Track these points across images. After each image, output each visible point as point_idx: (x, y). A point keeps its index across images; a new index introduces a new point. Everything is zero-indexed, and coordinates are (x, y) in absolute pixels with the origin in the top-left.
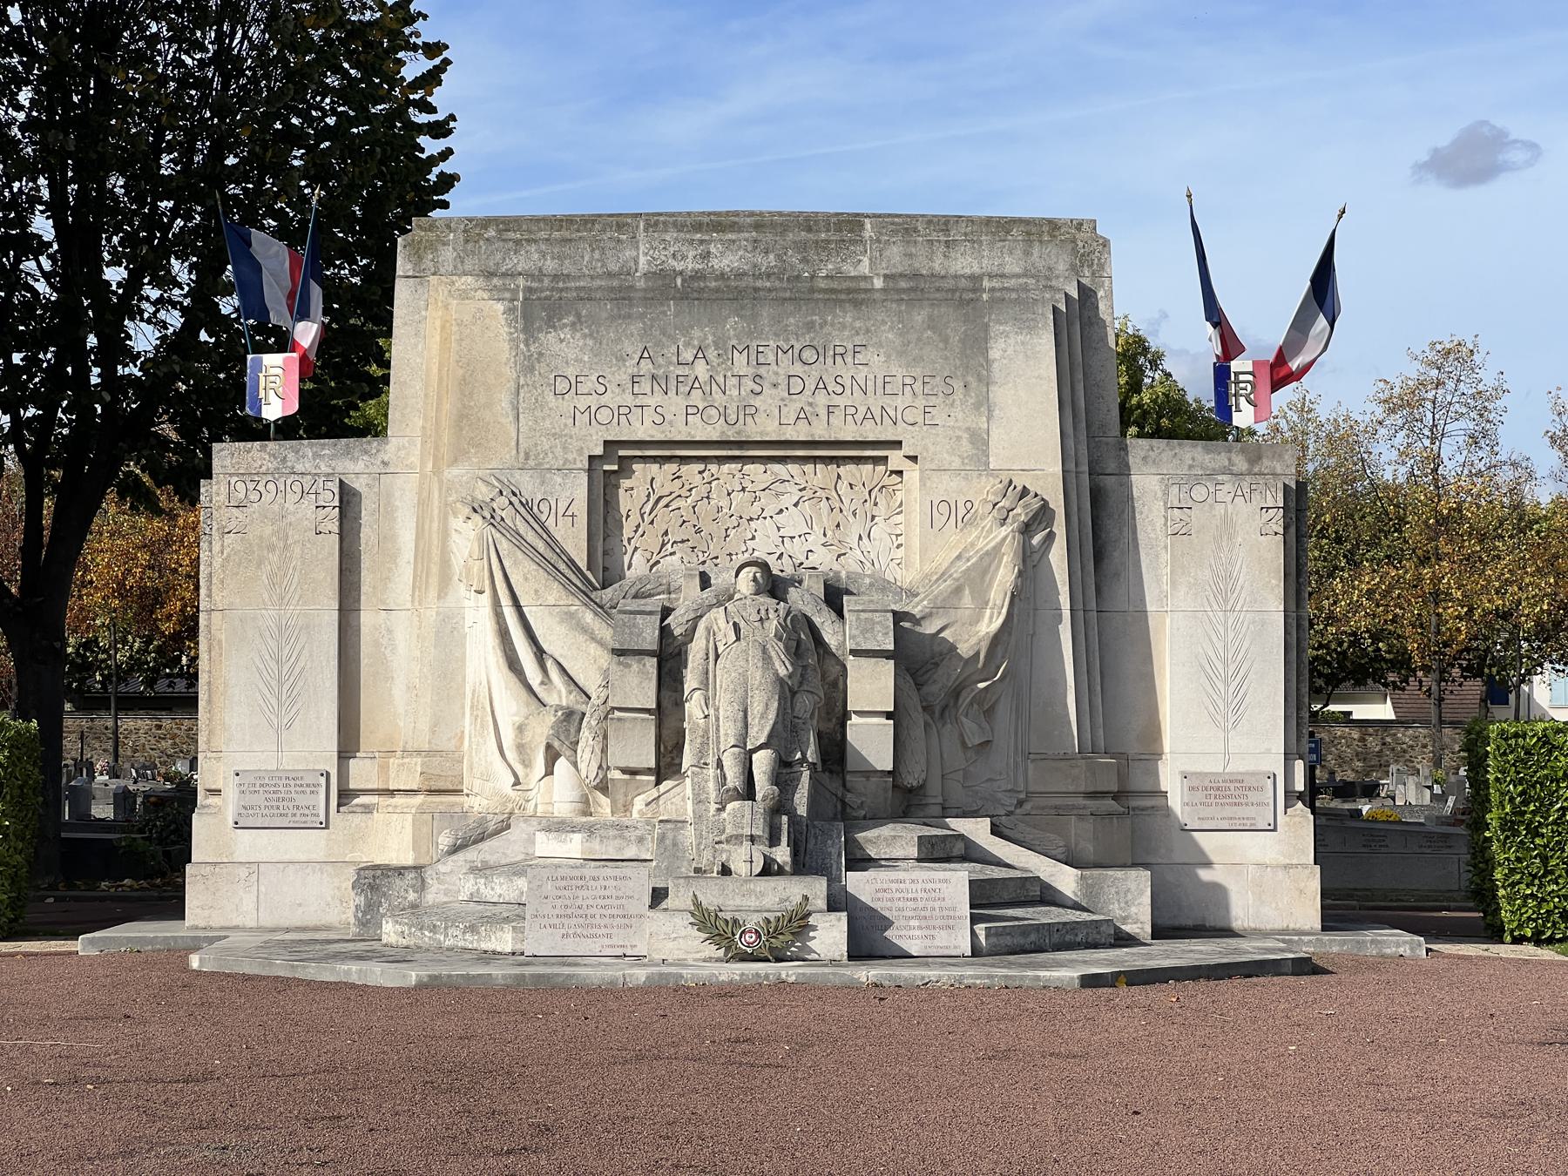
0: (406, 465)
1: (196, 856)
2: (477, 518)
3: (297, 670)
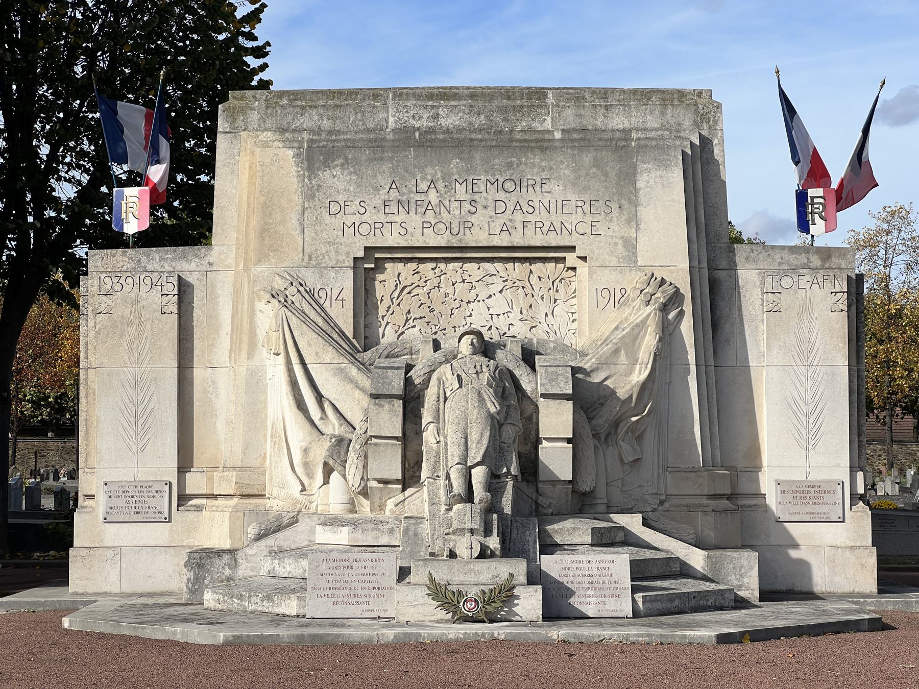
0: (224, 266)
2: (275, 302)
3: (148, 410)
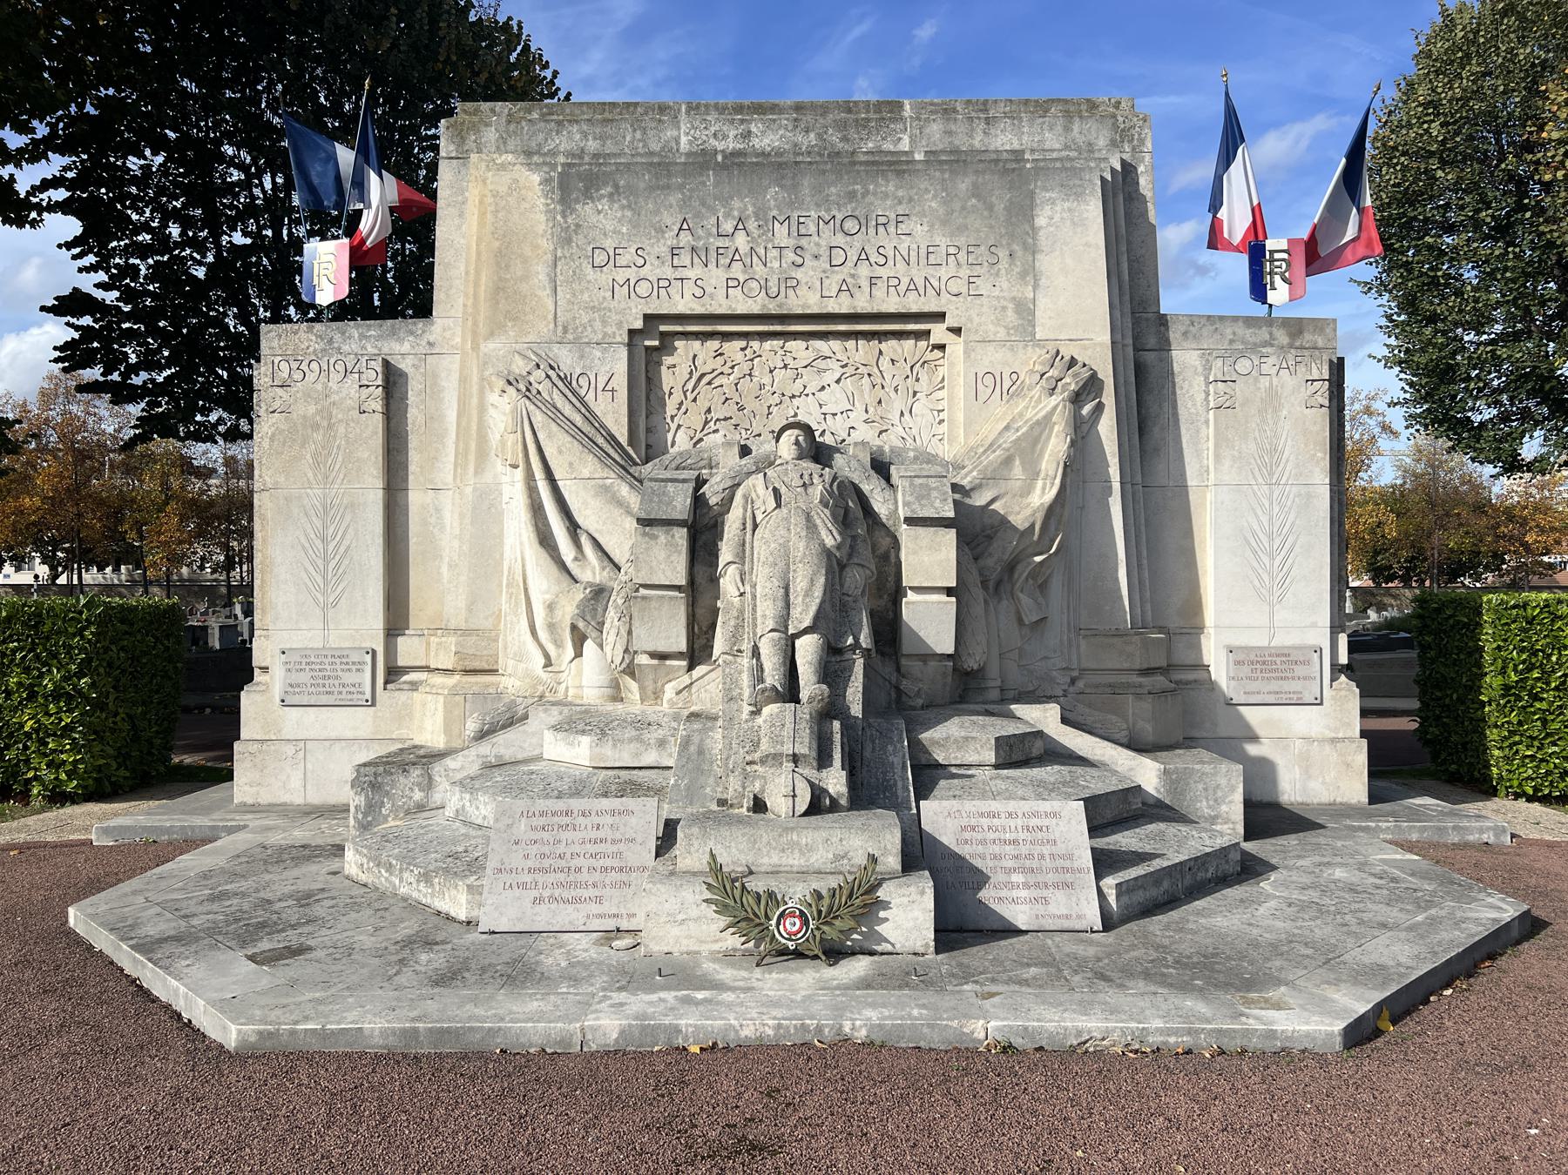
0: (450, 350)
1: (245, 733)
2: (511, 390)
3: (342, 549)
